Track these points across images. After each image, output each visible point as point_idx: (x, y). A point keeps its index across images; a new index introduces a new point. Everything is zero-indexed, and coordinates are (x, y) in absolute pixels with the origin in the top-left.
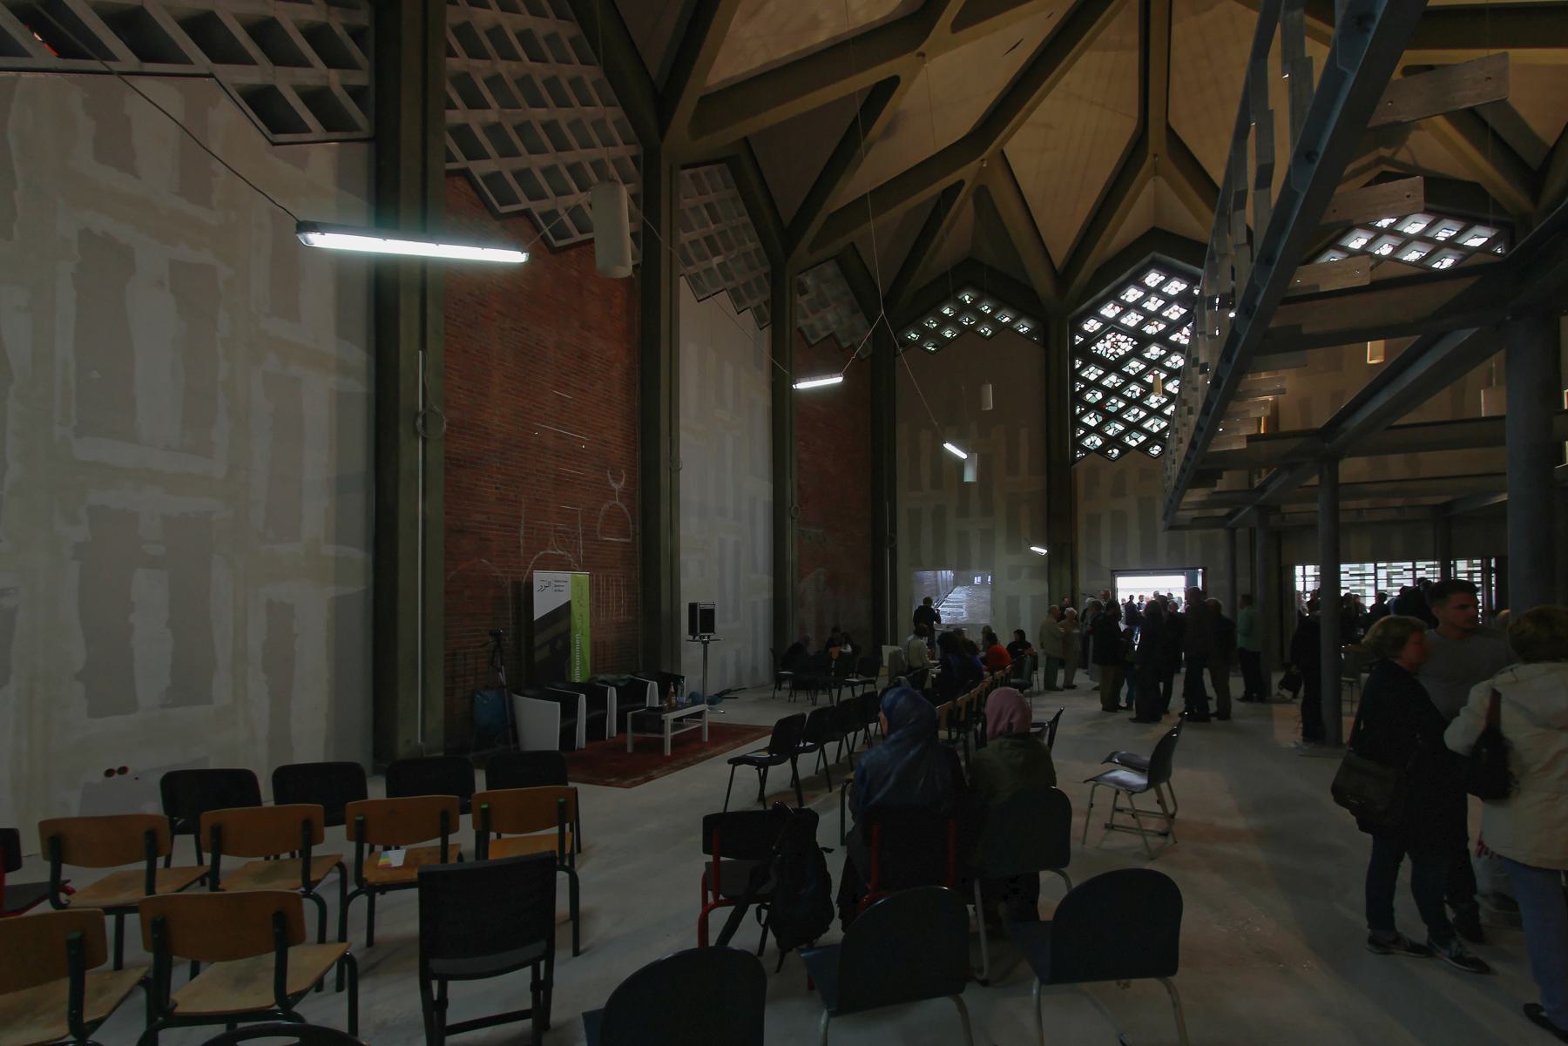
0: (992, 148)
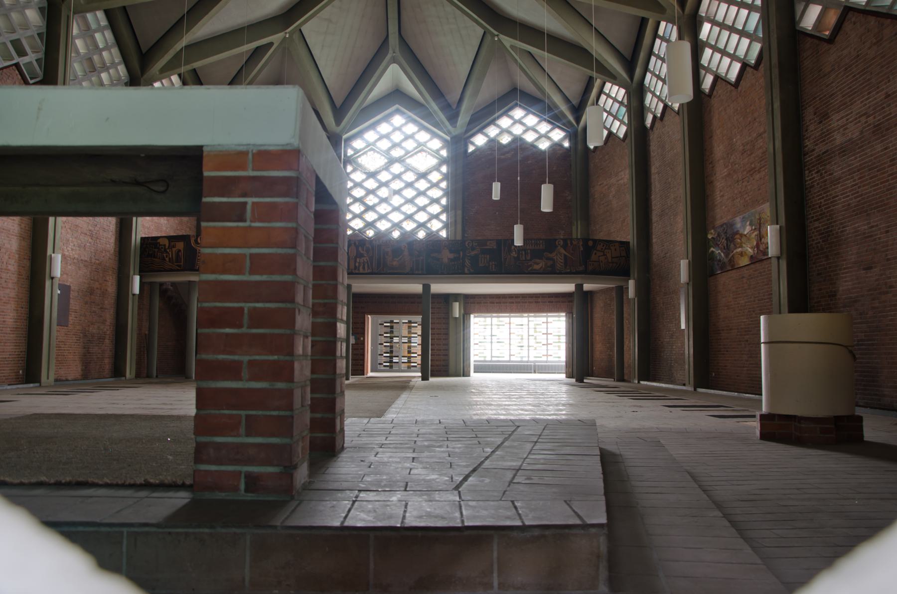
0: (295, 25)
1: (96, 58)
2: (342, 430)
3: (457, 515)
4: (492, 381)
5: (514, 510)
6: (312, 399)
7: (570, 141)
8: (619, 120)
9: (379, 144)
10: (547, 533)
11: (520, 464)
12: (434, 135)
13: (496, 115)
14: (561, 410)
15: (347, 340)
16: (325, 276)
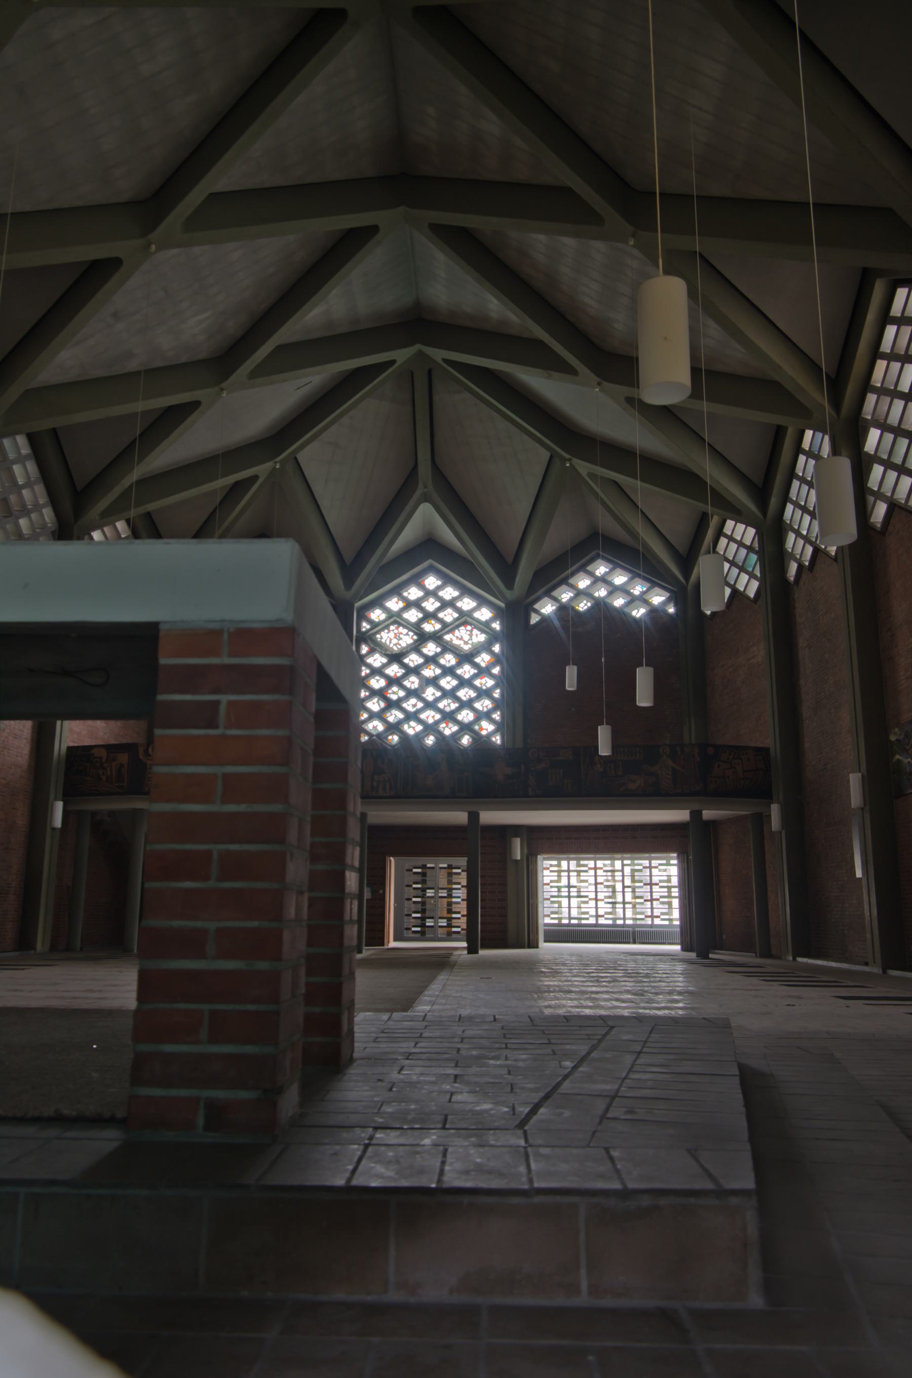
1: (13, 498)
2: (351, 1032)
3: (522, 1169)
4: (571, 955)
5: (610, 1165)
6: (307, 984)
7: (676, 605)
8: (747, 572)
9: (406, 615)
10: (663, 1201)
11: (616, 1087)
12: (482, 602)
13: (569, 571)
14: (677, 1001)
15: (360, 896)
16: (329, 804)
